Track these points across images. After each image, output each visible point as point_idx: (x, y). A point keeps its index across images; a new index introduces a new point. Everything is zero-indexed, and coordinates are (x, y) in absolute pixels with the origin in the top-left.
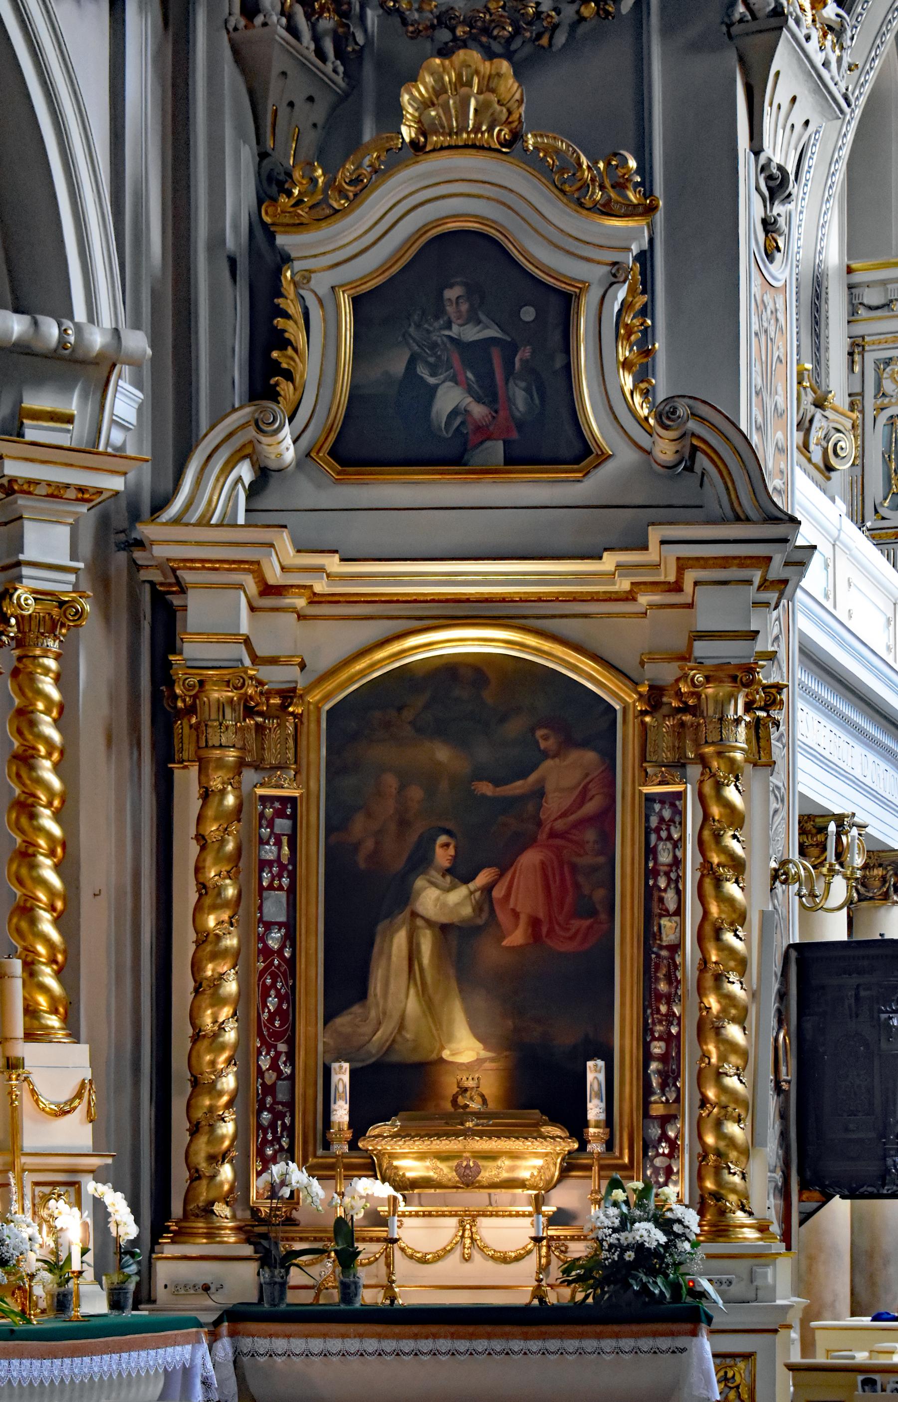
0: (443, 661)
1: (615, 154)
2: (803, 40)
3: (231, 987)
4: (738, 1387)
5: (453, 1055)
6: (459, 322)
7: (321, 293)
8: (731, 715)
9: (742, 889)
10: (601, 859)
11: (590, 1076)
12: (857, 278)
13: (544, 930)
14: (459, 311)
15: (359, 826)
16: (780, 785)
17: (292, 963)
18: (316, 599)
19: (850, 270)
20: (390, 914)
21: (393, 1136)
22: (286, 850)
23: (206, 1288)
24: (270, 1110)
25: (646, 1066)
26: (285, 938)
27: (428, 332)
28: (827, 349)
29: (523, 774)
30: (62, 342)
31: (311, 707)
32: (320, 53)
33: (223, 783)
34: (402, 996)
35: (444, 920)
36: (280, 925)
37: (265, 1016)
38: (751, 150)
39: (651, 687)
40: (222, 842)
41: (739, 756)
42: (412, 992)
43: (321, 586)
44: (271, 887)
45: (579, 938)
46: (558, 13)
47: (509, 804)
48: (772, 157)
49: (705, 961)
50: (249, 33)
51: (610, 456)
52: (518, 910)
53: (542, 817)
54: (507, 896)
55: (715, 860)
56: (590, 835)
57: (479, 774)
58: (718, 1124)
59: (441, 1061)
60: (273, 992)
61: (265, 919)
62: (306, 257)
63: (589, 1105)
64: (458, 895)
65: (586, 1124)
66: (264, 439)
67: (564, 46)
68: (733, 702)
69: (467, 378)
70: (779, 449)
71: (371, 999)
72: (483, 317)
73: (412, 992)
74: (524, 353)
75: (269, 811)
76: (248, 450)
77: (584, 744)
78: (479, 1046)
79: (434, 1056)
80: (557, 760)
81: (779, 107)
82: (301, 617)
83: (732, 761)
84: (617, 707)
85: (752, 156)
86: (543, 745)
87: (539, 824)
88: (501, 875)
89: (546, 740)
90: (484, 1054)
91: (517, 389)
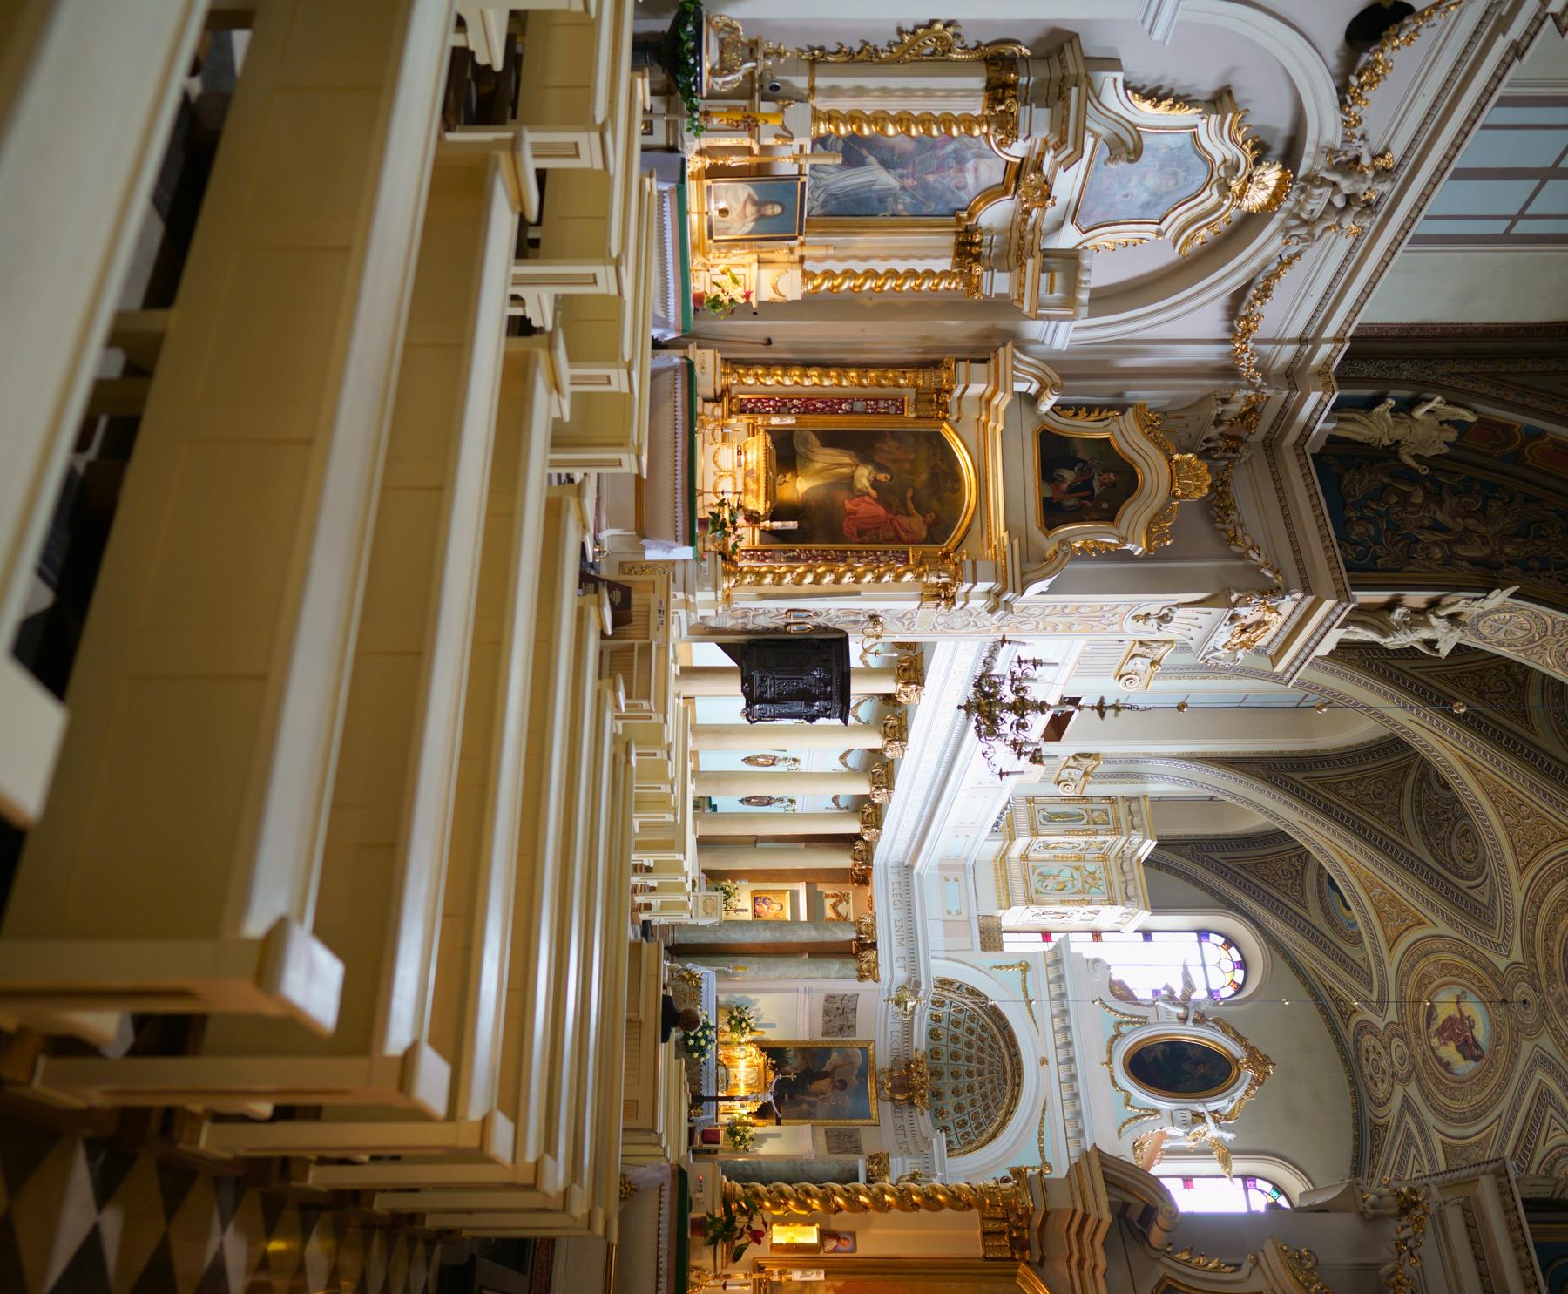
3: (826, 383)
10: (881, 539)
12: (1142, 800)
13: (852, 517)
15: (893, 444)
18: (985, 424)
19: (1145, 797)
21: (766, 445)
23: (703, 368)
28: (1110, 783)
30: (1081, 282)
40: (886, 378)
41: (925, 579)
43: (991, 424)
56: (891, 535)
57: (915, 491)
58: (771, 572)
64: (867, 484)
65: (771, 521)
74: (1089, 504)
75: (898, 404)
77: (929, 532)
82: (978, 420)
87: (896, 514)
89: (929, 518)
90: (800, 493)
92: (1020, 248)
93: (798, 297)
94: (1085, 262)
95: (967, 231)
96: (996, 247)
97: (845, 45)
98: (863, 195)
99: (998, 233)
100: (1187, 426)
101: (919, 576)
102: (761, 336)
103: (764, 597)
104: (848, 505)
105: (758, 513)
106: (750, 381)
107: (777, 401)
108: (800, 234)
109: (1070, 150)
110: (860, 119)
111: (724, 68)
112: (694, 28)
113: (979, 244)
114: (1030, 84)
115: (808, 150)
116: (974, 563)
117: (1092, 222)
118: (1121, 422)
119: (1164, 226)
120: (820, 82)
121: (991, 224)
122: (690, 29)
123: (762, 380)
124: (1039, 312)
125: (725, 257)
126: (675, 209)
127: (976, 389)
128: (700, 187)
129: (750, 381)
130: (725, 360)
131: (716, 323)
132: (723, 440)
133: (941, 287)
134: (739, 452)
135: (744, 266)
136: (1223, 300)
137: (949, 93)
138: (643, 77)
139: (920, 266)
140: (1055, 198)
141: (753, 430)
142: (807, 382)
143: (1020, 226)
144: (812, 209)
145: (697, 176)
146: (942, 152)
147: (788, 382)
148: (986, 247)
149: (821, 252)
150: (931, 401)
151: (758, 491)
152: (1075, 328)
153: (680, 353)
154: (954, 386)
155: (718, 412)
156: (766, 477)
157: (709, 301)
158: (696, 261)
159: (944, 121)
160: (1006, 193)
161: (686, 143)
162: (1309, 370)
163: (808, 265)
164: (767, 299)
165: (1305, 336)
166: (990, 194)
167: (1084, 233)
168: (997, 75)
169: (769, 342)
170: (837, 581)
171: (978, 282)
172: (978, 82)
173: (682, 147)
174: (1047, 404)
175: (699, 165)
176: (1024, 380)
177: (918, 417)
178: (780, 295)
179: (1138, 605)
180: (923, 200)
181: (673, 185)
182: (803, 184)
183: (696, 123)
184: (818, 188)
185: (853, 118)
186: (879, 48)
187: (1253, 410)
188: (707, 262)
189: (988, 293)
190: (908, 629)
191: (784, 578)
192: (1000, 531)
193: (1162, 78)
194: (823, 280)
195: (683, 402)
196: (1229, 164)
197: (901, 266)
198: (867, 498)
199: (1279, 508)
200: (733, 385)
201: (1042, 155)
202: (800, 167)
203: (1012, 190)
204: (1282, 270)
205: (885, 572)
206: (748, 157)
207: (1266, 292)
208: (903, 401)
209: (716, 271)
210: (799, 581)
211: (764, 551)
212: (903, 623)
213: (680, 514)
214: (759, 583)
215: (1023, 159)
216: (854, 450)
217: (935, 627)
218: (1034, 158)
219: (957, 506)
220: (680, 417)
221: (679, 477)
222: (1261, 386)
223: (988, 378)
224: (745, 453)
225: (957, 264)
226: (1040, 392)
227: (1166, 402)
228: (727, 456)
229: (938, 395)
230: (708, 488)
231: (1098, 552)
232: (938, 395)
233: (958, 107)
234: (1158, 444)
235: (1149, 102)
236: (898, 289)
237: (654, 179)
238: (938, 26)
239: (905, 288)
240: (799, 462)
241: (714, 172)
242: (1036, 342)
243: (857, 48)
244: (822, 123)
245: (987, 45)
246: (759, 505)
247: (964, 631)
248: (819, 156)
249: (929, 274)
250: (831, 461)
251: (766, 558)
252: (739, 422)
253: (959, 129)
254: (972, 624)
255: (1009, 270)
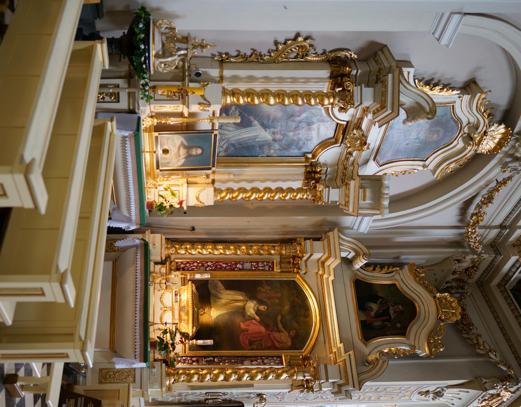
0: (310, 308)
1: (443, 345)
2: (478, 398)
4: (126, 379)
5: (213, 311)
6: (394, 309)
7: (395, 276)
8: (306, 375)
9: (260, 379)
10: (264, 347)
11: (209, 341)
13: (245, 333)
14: (396, 309)
15: (268, 288)
16: (285, 400)
17: (234, 270)
18: (322, 276)
20: (247, 295)
21: (192, 291)
22: (261, 268)
23: (154, 245)
24: (198, 265)
25: (212, 357)
26: (240, 268)
27: (390, 301)
29: (283, 327)
30: (384, 194)
31: (295, 276)
32: (447, 283)
33: (277, 249)
34: (227, 298)
35: (246, 308)
36: (243, 267)
37: (220, 264)
38: (448, 386)
39: (309, 357)
40: (263, 250)
41: (295, 377)
42: (228, 301)
43: (325, 276)
44: (252, 265)
45: (244, 342)
46: (472, 334)
47: (276, 324)
48: (446, 392)
49: (240, 369)
50: (453, 260)
51: (367, 346)
52: (250, 326)
53: (273, 332)
54: (253, 324)
55: (267, 371)
56: (270, 344)
58: (197, 373)
59: (211, 308)
60: (226, 266)
61: (244, 263)
62: (403, 273)
63: (201, 341)
64: (254, 313)
65: (197, 340)
66: (361, 257)
67: (464, 337)
68: (309, 375)
69: (380, 311)
70: (370, 398)
71: (226, 291)
72: (396, 314)
73: (228, 301)
74: (389, 325)
75: (270, 264)
76: (358, 254)
77: (293, 342)
78: (215, 317)
79: (212, 306)
80: (288, 335)
81: (459, 394)
82: (317, 273)
83: (294, 376)
84: (303, 350)
85: (446, 385)
86: (291, 332)
87: (272, 331)
88: (258, 322)
89: (293, 333)
90: (213, 318)
91: (379, 323)
92: (344, 175)
93: (212, 203)
94: (386, 182)
95: (312, 165)
96: (329, 174)
97: (241, 51)
98: (250, 144)
99: (331, 166)
100: (435, 274)
101: (291, 376)
102: (188, 225)
103: (193, 388)
104: (243, 326)
105: (189, 334)
106: (183, 252)
107: (199, 263)
108: (213, 166)
109: (389, 111)
110: (253, 94)
111: (165, 53)
112: (144, 25)
113: (319, 173)
114: (358, 74)
115: (218, 114)
116: (326, 366)
117: (385, 161)
118: (401, 274)
119: (427, 163)
120: (227, 73)
121: (326, 161)
122: (141, 26)
123: (190, 251)
124: (359, 212)
125: (167, 180)
126: (134, 148)
127: (317, 256)
128: (150, 137)
129: (183, 252)
130: (167, 239)
131: (162, 218)
132: (166, 288)
133: (297, 198)
134: (176, 295)
135: (178, 185)
136: (459, 205)
137: (307, 80)
138: (102, 43)
139: (285, 185)
140: (369, 144)
141: (184, 282)
142: (216, 252)
143: (343, 161)
144: (220, 152)
145: (148, 130)
146: (298, 119)
147: (205, 252)
148: (323, 174)
149: (226, 177)
150: (290, 262)
151: (188, 320)
152: (374, 220)
153: (140, 236)
154: (304, 255)
155: (163, 270)
156: (193, 311)
157: (157, 207)
158: (148, 182)
159: (306, 95)
160: (336, 142)
161: (141, 108)
162: (507, 244)
163: (217, 185)
164: (193, 205)
165: (505, 224)
166: (325, 144)
167: (381, 166)
168: (338, 69)
169: (193, 229)
170: (239, 379)
171: (320, 194)
172: (325, 73)
173: (138, 110)
174: (360, 263)
175: (150, 123)
176: (345, 251)
177: (282, 272)
178: (201, 202)
179: (422, 387)
180: (286, 147)
181: (131, 132)
182: (216, 136)
183: (147, 93)
184: (224, 140)
185: (248, 93)
186: (263, 53)
187: (474, 266)
188: (156, 183)
189: (326, 201)
190: (281, 400)
191: (206, 378)
192: (338, 345)
193: (435, 74)
194: (227, 194)
195: (141, 267)
196: (471, 125)
197: (273, 186)
198: (253, 321)
199: (496, 324)
200: (172, 254)
201: (361, 119)
202: (213, 124)
203: (340, 141)
204: (500, 187)
205: (270, 373)
206: (181, 118)
207: (489, 199)
208: (273, 263)
209: (161, 188)
210: (215, 379)
211: (192, 357)
212: (278, 398)
213: (138, 340)
214: (189, 381)
215: (348, 122)
216: (245, 292)
217: (297, 399)
218: (356, 121)
219: (308, 326)
220: (139, 277)
221: (138, 315)
222: (481, 253)
223: (324, 250)
224: (180, 296)
225: (307, 184)
226: (354, 258)
227: (424, 261)
228: (168, 298)
229: (294, 259)
230: (157, 320)
231: (399, 356)
232: (294, 259)
233: (314, 88)
234: (426, 288)
235: (428, 87)
236: (271, 198)
237: (114, 123)
238: (300, 39)
239: (276, 198)
240: (212, 299)
241: (159, 128)
242: (348, 228)
243: (249, 53)
244: (228, 97)
245: (330, 52)
246: (189, 329)
247: (314, 401)
248: (224, 118)
249: (290, 190)
250: (232, 299)
251: (193, 361)
252: (176, 277)
253: (315, 100)
254: (320, 397)
255: (338, 187)
